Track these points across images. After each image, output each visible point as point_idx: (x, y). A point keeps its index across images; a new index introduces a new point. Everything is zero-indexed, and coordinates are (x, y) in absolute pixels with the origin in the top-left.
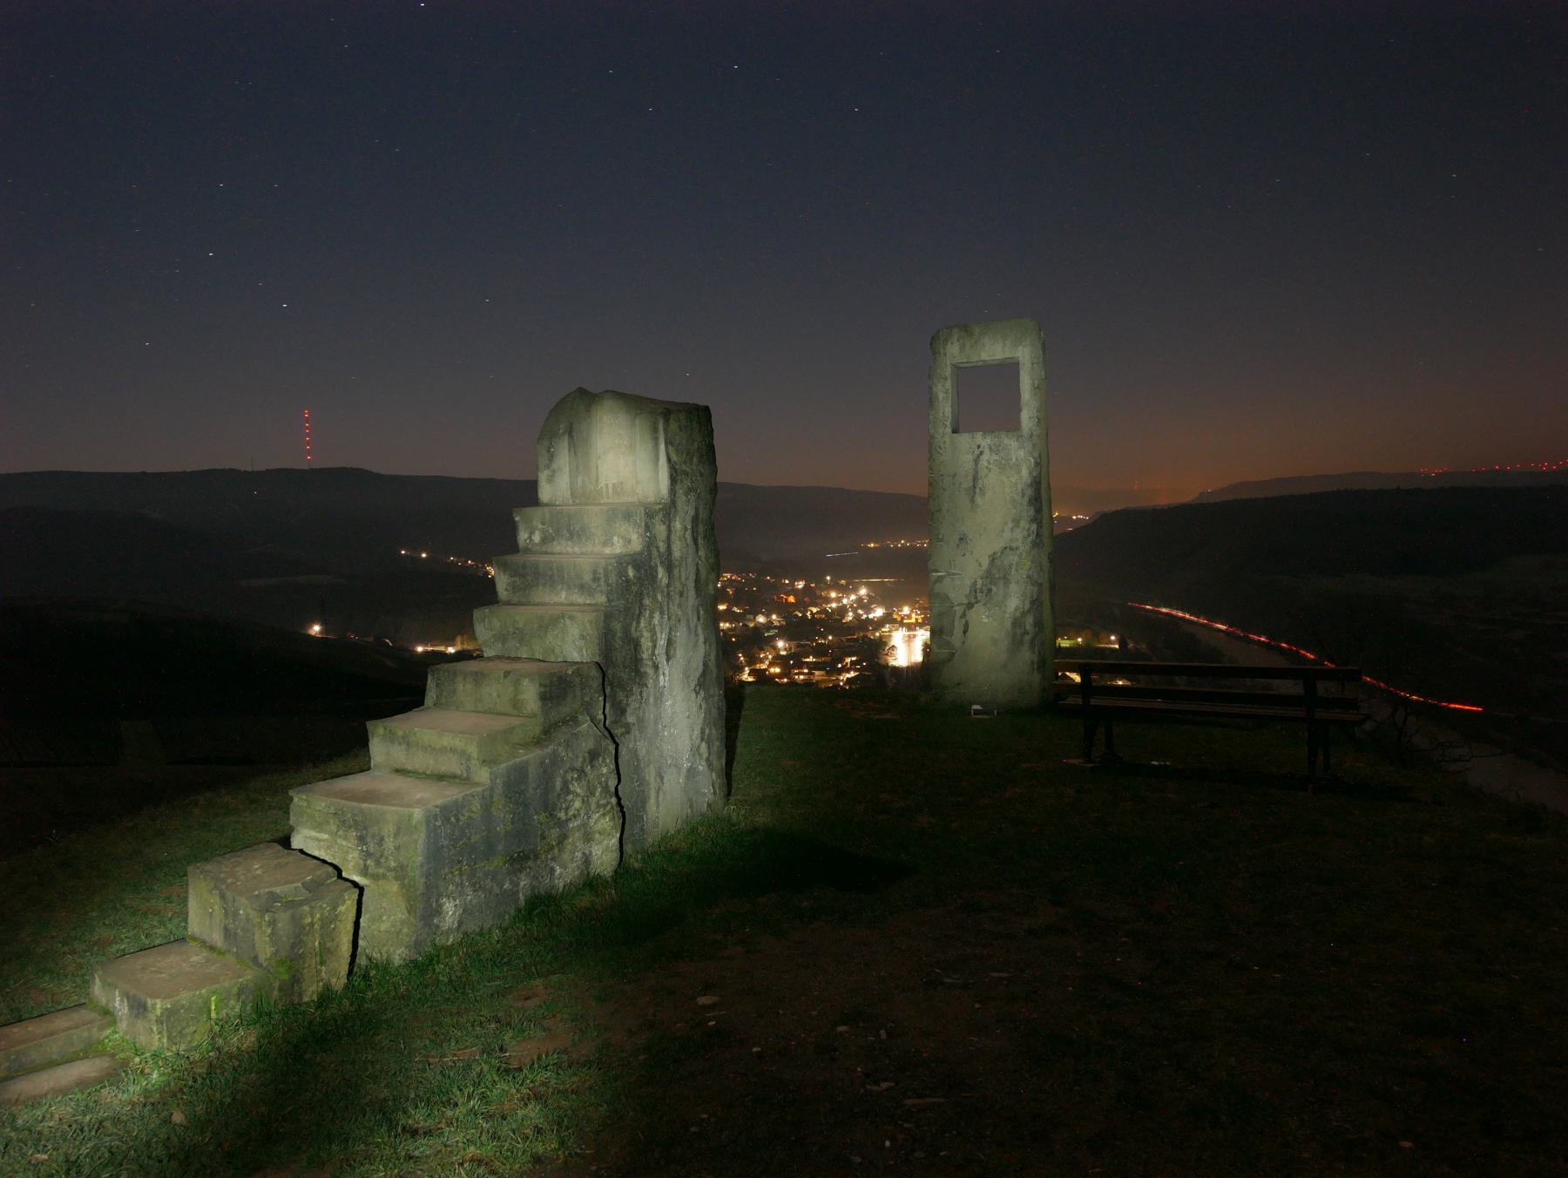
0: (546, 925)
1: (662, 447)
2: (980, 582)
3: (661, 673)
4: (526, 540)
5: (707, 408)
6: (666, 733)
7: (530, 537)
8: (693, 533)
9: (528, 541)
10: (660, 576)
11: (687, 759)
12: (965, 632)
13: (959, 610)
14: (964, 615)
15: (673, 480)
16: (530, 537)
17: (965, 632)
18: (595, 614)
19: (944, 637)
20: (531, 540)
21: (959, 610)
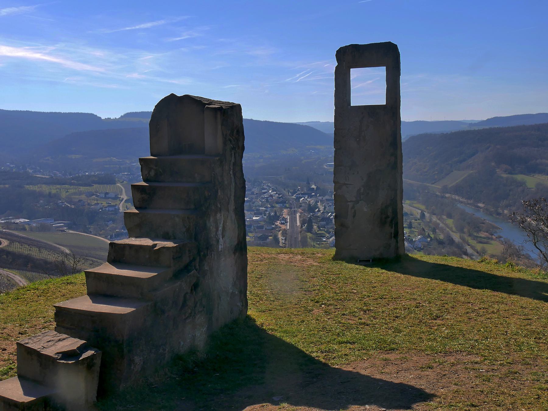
0: (504, 268)
1: (220, 127)
2: (362, 189)
3: (220, 244)
4: (146, 175)
5: (239, 106)
6: (222, 275)
7: (149, 173)
8: (233, 171)
9: (148, 175)
10: (219, 194)
11: (231, 288)
12: (354, 216)
13: (351, 204)
14: (353, 207)
15: (225, 144)
16: (149, 173)
17: (354, 216)
18: (461, 241)
19: (437, 233)
20: (149, 175)
21: (351, 204)
